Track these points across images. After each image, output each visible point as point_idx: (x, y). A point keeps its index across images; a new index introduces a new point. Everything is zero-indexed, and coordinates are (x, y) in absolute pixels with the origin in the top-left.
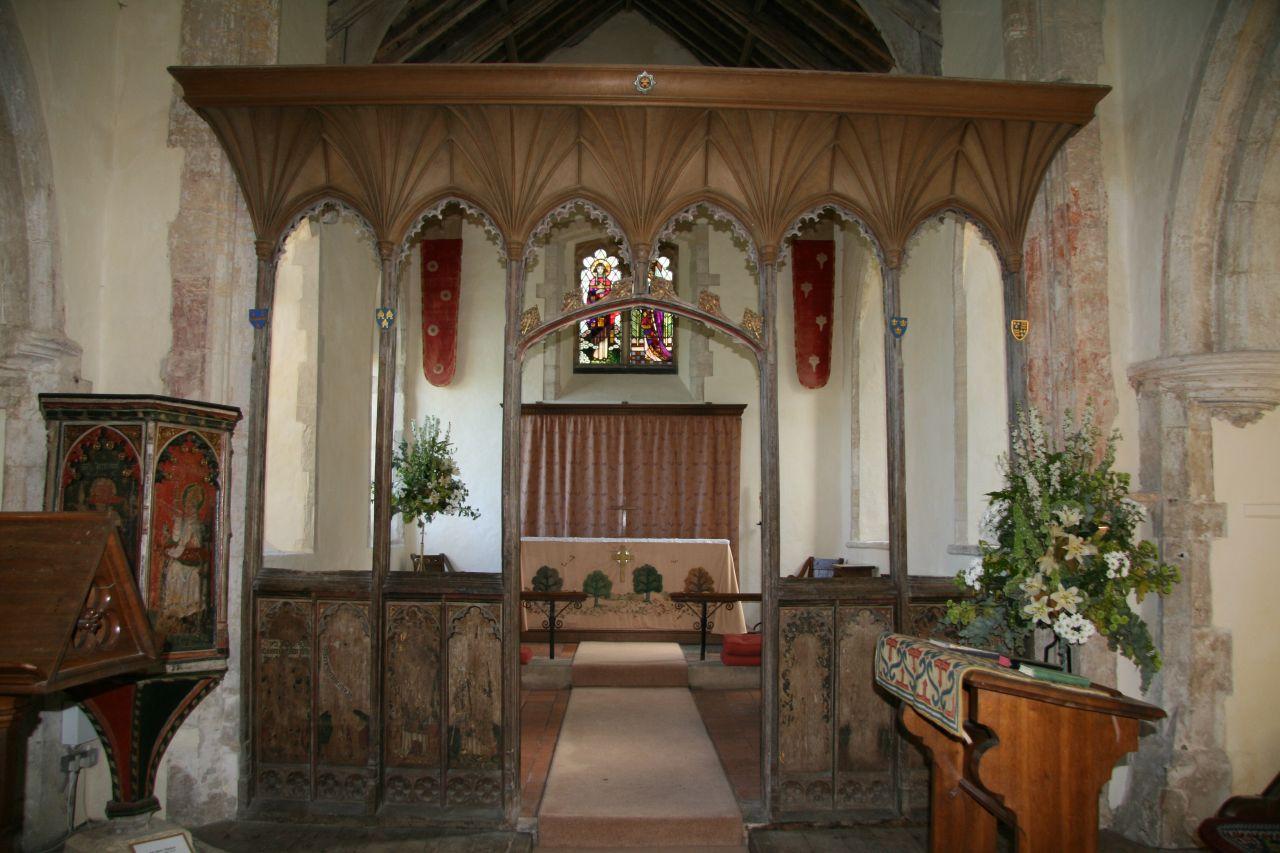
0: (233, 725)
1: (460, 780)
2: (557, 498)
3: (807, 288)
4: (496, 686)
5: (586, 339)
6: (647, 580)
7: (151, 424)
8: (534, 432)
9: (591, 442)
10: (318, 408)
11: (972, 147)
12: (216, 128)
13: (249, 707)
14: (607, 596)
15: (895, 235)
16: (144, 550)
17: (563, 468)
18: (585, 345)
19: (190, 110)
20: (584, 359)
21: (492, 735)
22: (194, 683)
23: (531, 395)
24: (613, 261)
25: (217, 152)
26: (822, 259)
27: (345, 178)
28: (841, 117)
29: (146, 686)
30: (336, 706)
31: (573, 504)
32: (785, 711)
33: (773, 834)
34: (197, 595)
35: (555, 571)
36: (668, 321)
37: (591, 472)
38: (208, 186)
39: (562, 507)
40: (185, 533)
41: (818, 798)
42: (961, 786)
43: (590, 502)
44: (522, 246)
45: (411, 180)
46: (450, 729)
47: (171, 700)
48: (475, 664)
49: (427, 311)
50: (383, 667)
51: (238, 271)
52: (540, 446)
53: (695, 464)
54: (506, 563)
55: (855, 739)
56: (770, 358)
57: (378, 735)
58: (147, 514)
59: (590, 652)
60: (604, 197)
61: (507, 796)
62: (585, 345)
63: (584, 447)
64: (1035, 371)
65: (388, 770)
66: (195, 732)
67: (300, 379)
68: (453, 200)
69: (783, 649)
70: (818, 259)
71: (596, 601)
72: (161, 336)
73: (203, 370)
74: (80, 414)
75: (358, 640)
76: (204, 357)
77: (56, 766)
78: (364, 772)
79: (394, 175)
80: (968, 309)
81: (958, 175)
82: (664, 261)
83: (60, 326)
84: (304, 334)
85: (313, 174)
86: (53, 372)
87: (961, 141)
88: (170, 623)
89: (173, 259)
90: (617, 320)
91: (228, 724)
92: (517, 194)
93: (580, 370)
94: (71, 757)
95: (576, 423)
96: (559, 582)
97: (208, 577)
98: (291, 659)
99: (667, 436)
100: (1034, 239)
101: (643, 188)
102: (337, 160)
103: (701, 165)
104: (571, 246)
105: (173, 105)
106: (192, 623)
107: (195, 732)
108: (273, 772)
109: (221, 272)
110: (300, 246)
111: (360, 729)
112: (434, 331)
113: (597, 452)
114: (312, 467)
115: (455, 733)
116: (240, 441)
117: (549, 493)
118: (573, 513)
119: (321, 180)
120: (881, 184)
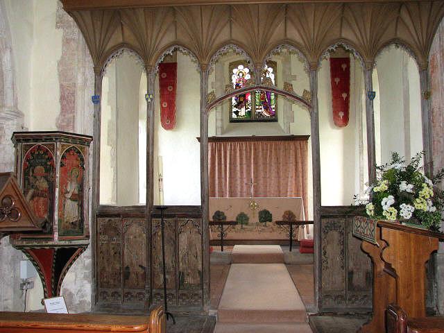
0: (89, 272)
1: (184, 295)
2: (223, 180)
3: (337, 80)
4: (199, 253)
5: (235, 107)
6: (265, 216)
7: (58, 143)
8: (212, 150)
9: (238, 154)
10: (117, 140)
11: (404, 14)
12: (76, 20)
13: (95, 264)
14: (247, 224)
15: (372, 52)
16: (57, 194)
17: (226, 166)
18: (234, 109)
19: (65, 12)
20: (234, 116)
21: (198, 275)
22: (77, 249)
23: (211, 133)
24: (247, 70)
25: (77, 30)
26: (344, 66)
27: (130, 38)
28: (344, 5)
29: (58, 249)
30: (132, 264)
31: (230, 183)
32: (324, 264)
33: (318, 317)
34: (77, 215)
35: (223, 213)
36: (273, 97)
37: (238, 168)
38: (73, 45)
39: (226, 185)
40: (72, 188)
41: (339, 303)
42: (384, 271)
43: (239, 182)
44: (207, 65)
45: (159, 39)
46: (180, 273)
47: (65, 257)
48: (190, 245)
49: (162, 96)
50: (151, 246)
51: (87, 80)
52: (211, 170)
53: (287, 163)
54: (203, 201)
55: (355, 277)
56: (315, 111)
57: (149, 276)
58: (58, 180)
59: (239, 249)
60: (241, 43)
61: (205, 300)
62: (234, 109)
63: (235, 156)
64: (434, 114)
65: (154, 290)
66: (73, 274)
67: (108, 127)
68: (177, 46)
69: (323, 237)
70: (342, 66)
71: (242, 226)
72: (57, 108)
73: (74, 121)
74: (29, 140)
75: (140, 235)
76: (74, 116)
77: (18, 288)
78: (144, 292)
79: (152, 37)
80: (410, 87)
81: (398, 27)
82: (271, 70)
83: (16, 106)
84: (109, 107)
85: (117, 38)
86: (14, 125)
87: (399, 11)
88: (67, 224)
89: (60, 75)
90: (249, 98)
91: (87, 271)
92: (204, 43)
93: (232, 121)
94: (24, 284)
95: (231, 145)
96: (225, 218)
97: (81, 206)
98: (113, 244)
99: (273, 150)
100: (434, 55)
101: (259, 38)
102: (127, 32)
103: (283, 28)
104: (227, 64)
105: (58, 11)
106: (75, 225)
107: (73, 274)
108: (106, 292)
109: (80, 80)
110: (111, 69)
111: (142, 273)
112: (165, 105)
113: (241, 159)
114: (114, 166)
115: (182, 274)
116: (91, 150)
117: (220, 178)
118: (230, 187)
119: (121, 40)
120: (362, 30)
